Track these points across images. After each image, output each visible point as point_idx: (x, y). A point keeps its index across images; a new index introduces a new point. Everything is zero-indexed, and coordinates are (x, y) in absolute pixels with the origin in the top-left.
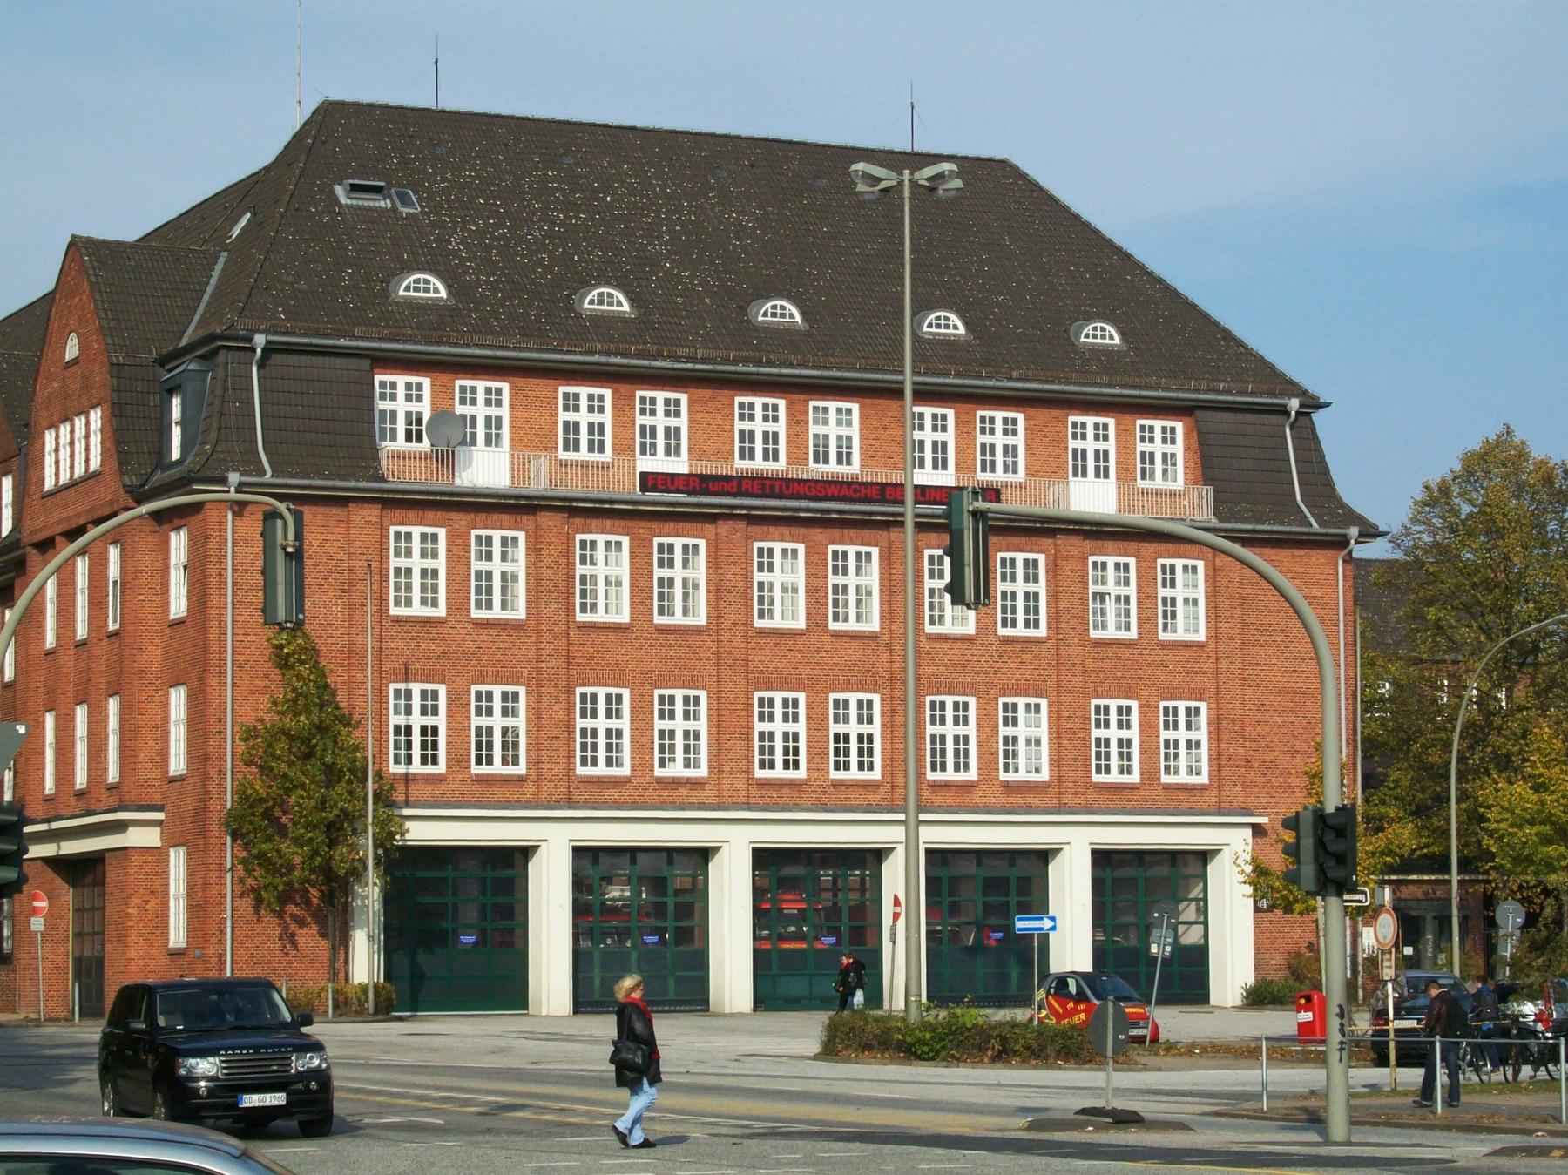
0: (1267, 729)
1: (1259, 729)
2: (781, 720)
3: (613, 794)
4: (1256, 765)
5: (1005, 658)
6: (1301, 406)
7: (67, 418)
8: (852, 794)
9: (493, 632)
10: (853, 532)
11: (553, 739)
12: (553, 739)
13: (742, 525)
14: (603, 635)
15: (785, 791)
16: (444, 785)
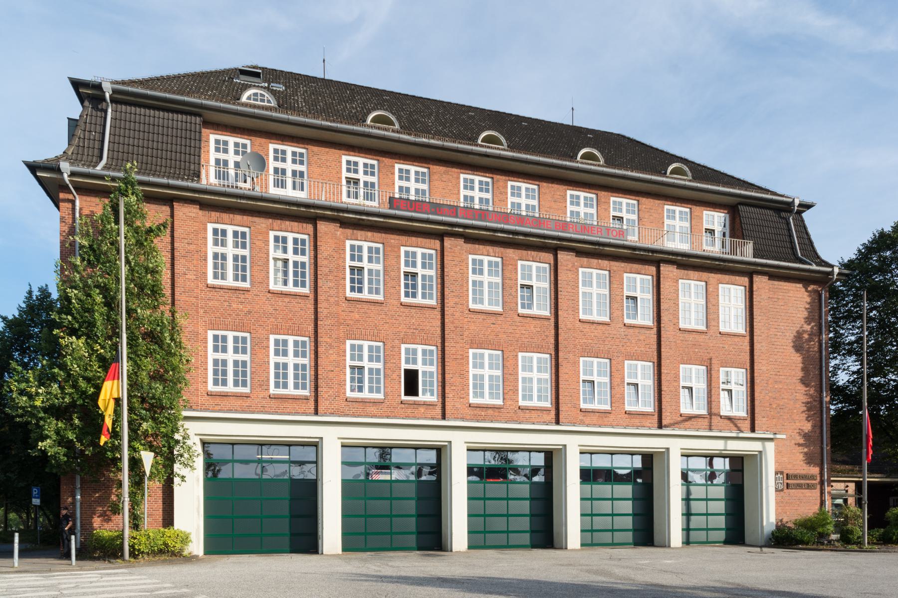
3: (372, 409)
9: (287, 300)
10: (534, 253)
13: (461, 241)
16: (249, 400)
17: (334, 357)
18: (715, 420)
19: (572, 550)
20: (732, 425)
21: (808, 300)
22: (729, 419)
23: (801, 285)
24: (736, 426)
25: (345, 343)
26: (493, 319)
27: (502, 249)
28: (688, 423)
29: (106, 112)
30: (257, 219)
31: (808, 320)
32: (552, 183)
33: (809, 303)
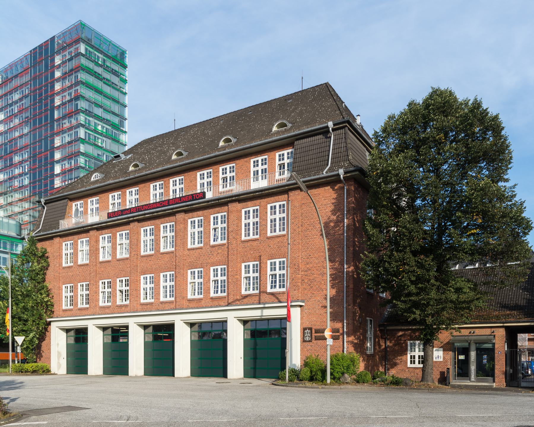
0: (311, 265)
1: (308, 266)
2: (192, 279)
3: (107, 311)
4: (306, 281)
5: (213, 253)
6: (334, 125)
7: (180, 197)
8: (166, 305)
10: (167, 219)
11: (178, 289)
12: (178, 289)
13: (136, 223)
14: (105, 264)
15: (148, 306)
17: (94, 289)
18: (264, 297)
19: (177, 378)
20: (274, 298)
21: (335, 196)
22: (272, 294)
23: (329, 187)
24: (277, 298)
25: (99, 282)
26: (150, 258)
27: (154, 221)
28: (245, 300)
29: (330, 137)
30: (75, 237)
31: (334, 212)
32: (190, 172)
33: (336, 198)
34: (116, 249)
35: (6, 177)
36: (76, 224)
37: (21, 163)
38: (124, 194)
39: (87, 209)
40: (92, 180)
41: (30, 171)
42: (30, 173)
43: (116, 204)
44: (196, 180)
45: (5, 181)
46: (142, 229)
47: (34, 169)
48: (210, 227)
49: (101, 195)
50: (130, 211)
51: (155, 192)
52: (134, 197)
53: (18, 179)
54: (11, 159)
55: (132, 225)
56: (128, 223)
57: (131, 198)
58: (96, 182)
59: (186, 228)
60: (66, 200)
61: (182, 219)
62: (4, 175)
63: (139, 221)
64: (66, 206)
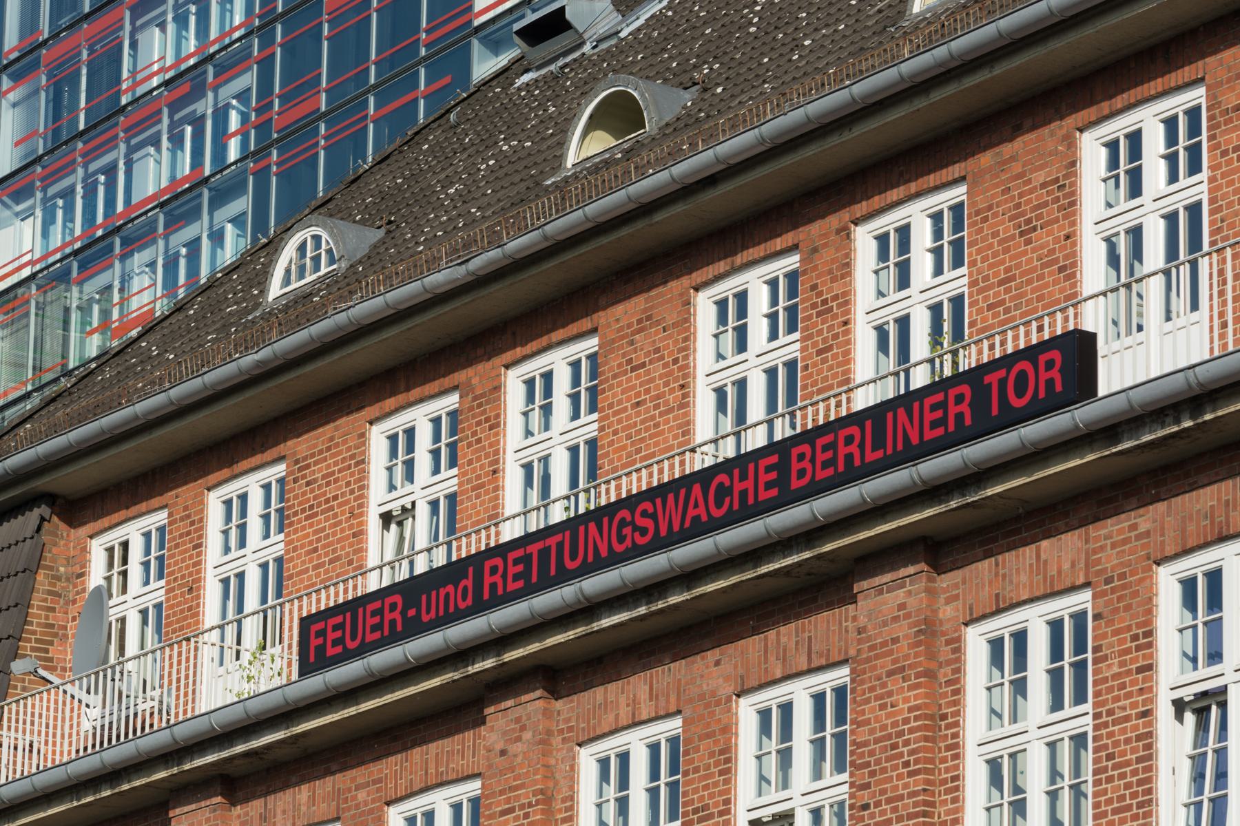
10: (786, 634)
13: (532, 705)
32: (1017, 131)
34: (1148, 757)
35: (56, 239)
36: (104, 737)
37: (186, 83)
38: (483, 415)
39: (194, 588)
40: (275, 289)
41: (262, 152)
42: (262, 176)
43: (423, 511)
44: (1070, 205)
45: (51, 276)
46: (587, 761)
47: (298, 133)
48: (1148, 691)
49: (300, 445)
50: (415, 601)
51: (729, 364)
52: (567, 429)
53: (156, 252)
54: (107, 66)
55: (502, 718)
56: (458, 711)
57: (540, 438)
58: (301, 306)
59: (941, 723)
60: (33, 516)
61: (903, 630)
62: (48, 222)
63: (558, 676)
64: (30, 570)
